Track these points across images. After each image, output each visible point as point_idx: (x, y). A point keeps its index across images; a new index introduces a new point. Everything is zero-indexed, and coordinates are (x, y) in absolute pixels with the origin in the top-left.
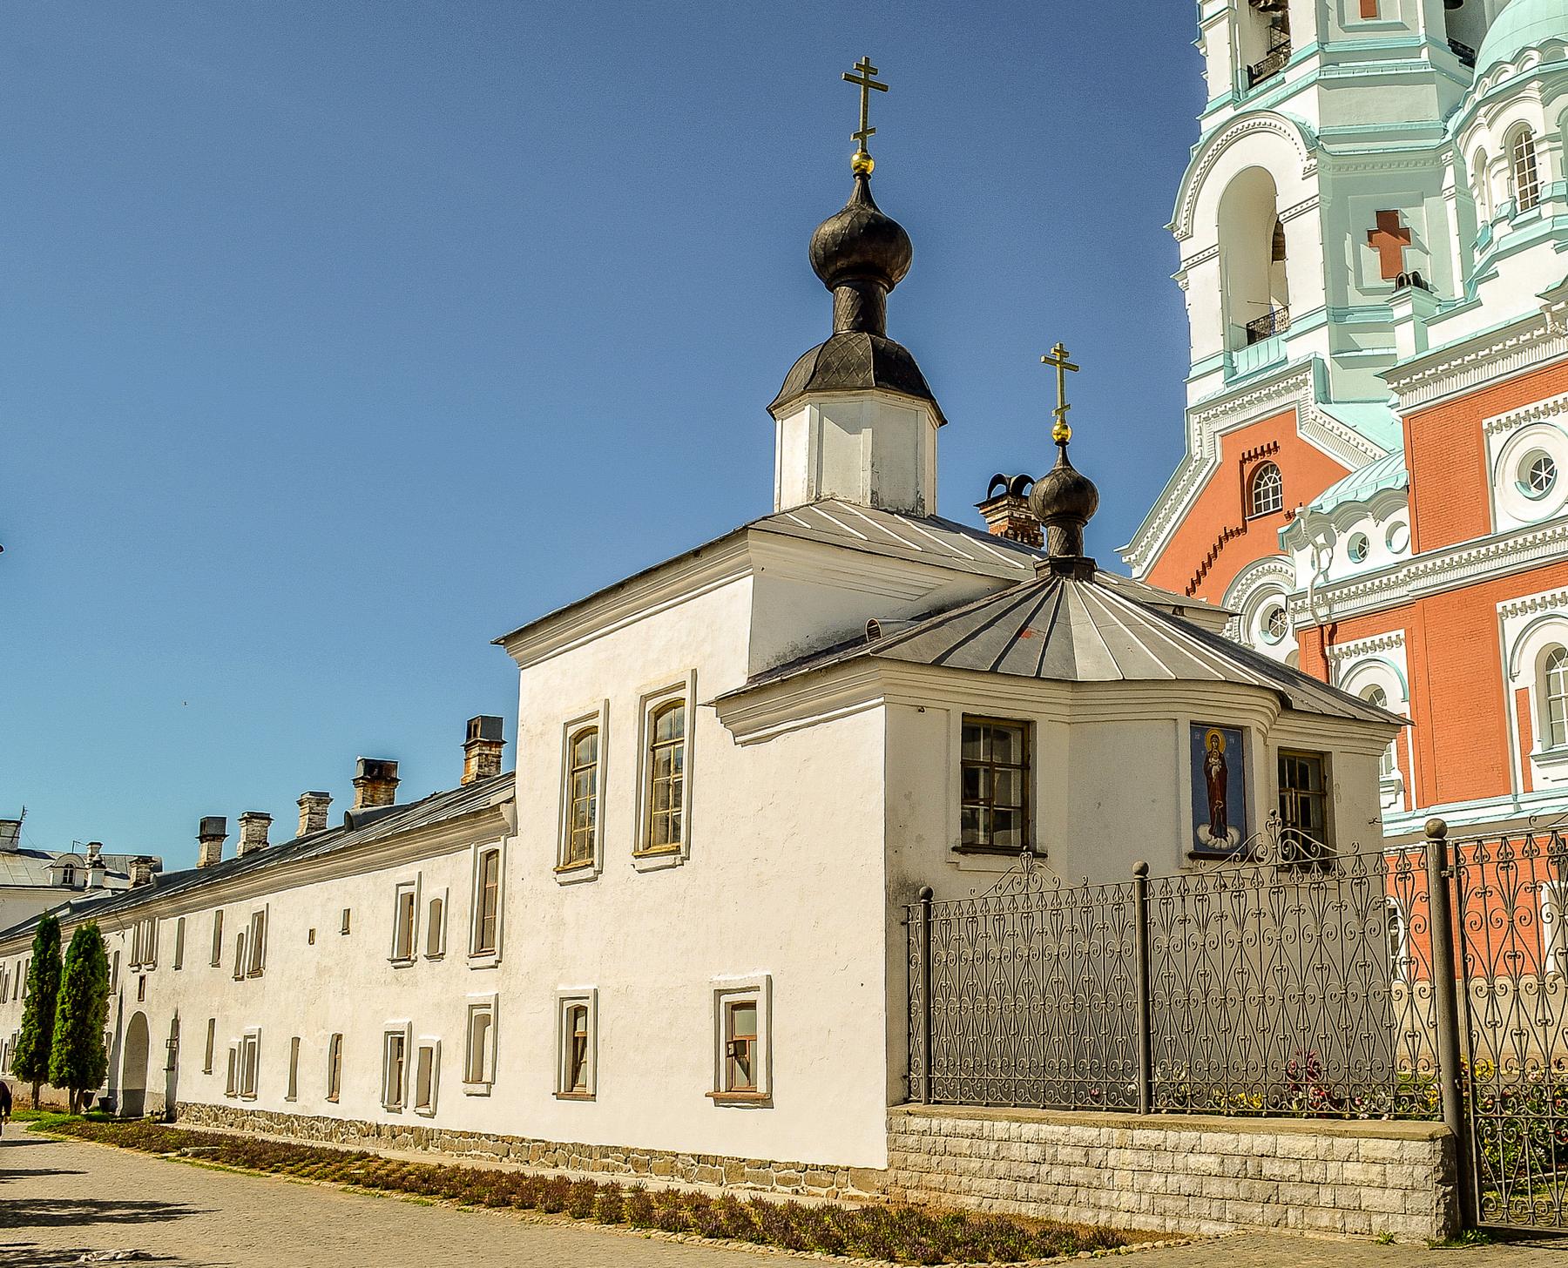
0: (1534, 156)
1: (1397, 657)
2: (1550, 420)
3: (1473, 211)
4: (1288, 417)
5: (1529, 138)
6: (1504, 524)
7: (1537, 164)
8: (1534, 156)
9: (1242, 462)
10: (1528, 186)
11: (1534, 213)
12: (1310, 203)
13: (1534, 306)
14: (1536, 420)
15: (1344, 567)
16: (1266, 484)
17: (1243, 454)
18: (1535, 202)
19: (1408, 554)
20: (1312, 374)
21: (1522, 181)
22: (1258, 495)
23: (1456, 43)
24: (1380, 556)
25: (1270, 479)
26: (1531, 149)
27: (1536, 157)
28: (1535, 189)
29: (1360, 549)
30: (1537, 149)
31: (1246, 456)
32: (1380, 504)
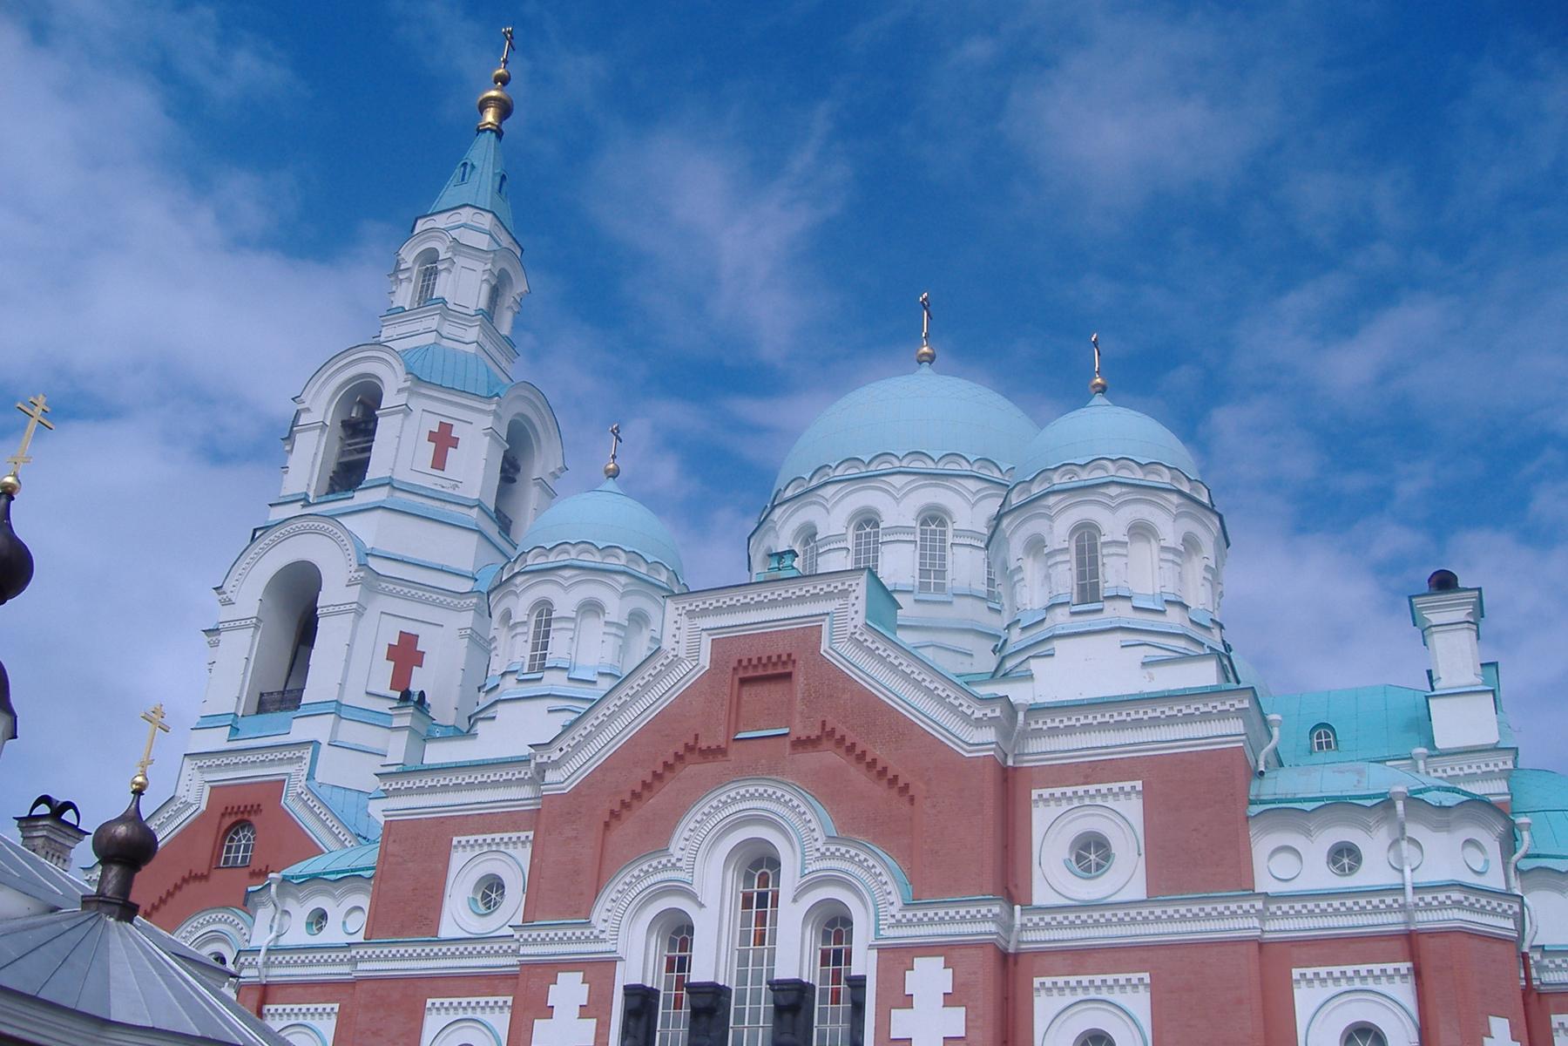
0: (546, 654)
1: (524, 855)
2: (511, 850)
3: (609, 1003)
4: (278, 786)
5: (550, 613)
6: (446, 931)
7: (551, 637)
8: (546, 654)
9: (223, 815)
10: (539, 652)
11: (539, 676)
12: (348, 607)
13: (526, 751)
14: (502, 848)
15: (297, 934)
16: (240, 840)
17: (227, 808)
18: (543, 668)
19: (359, 938)
20: (310, 754)
21: (535, 648)
22: (229, 848)
23: (500, 511)
24: (332, 934)
25: (244, 836)
26: (548, 623)
27: (548, 655)
28: (544, 657)
29: (320, 918)
30: (554, 626)
31: (229, 810)
32: (349, 878)
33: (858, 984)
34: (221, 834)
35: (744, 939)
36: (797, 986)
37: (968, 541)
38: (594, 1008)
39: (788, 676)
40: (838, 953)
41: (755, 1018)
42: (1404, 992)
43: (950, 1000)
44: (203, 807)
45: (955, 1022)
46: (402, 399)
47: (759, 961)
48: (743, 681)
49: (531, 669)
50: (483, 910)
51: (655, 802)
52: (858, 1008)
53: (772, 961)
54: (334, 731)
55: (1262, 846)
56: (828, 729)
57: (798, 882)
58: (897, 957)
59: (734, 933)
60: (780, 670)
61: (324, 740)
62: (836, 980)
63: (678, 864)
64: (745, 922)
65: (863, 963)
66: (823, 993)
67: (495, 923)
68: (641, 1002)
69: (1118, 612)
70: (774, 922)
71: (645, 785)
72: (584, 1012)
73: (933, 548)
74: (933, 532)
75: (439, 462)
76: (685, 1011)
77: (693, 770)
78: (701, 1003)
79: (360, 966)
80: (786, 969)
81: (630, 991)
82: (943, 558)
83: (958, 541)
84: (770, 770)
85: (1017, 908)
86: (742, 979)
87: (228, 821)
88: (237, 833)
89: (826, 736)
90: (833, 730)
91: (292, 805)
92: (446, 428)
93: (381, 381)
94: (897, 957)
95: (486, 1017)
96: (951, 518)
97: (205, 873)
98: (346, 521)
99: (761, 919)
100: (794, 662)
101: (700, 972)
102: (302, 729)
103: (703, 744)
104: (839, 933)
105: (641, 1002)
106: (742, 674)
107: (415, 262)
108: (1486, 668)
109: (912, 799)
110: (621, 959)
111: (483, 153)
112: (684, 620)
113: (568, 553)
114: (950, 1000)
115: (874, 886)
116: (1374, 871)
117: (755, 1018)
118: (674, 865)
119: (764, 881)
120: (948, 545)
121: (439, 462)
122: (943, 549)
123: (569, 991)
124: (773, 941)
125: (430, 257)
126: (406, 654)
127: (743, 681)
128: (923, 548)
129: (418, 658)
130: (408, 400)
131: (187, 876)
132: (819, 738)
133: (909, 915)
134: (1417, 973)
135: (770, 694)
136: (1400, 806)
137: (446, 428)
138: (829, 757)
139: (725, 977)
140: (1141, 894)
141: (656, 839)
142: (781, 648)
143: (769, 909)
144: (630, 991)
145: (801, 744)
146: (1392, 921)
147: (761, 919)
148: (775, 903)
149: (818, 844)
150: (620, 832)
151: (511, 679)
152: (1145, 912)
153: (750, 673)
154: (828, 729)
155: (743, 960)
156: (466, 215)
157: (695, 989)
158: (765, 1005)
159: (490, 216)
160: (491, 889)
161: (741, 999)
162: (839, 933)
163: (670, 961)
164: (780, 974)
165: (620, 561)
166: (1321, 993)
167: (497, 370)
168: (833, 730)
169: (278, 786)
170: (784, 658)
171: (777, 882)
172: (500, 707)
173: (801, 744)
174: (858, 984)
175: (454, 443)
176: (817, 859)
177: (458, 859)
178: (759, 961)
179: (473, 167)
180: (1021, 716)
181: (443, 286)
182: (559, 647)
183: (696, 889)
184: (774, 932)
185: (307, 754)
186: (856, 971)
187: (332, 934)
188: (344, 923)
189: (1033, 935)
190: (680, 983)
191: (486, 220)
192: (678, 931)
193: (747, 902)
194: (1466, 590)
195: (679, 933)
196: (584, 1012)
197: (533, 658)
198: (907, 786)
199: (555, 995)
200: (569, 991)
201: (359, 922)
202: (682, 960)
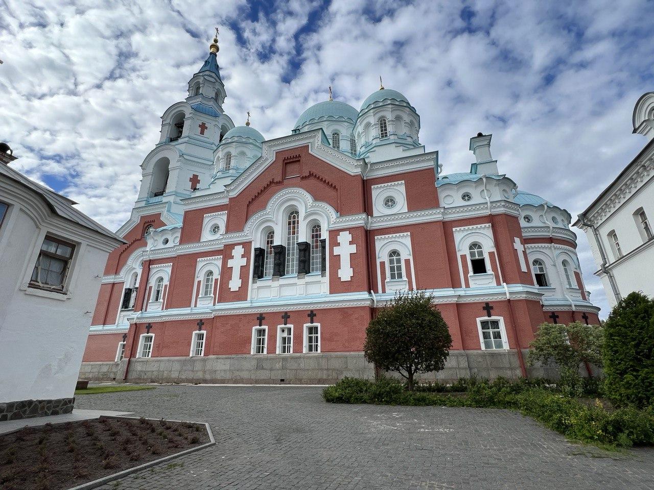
26: (230, 158)
29: (166, 241)
33: (324, 241)
35: (289, 234)
39: (299, 161)
40: (317, 235)
42: (489, 233)
43: (351, 243)
45: (353, 249)
47: (293, 239)
48: (286, 164)
49: (226, 170)
51: (262, 198)
52: (324, 248)
53: (297, 237)
55: (442, 195)
58: (334, 233)
62: (317, 242)
64: (289, 229)
65: (325, 235)
67: (217, 236)
68: (260, 253)
70: (298, 228)
72: (243, 256)
75: (202, 133)
77: (273, 187)
81: (256, 250)
84: (294, 186)
85: (369, 217)
86: (289, 244)
87: (146, 225)
88: (149, 228)
94: (334, 233)
95: (215, 262)
98: (177, 146)
99: (294, 228)
101: (277, 242)
103: (275, 181)
104: (317, 230)
105: (260, 253)
108: (477, 172)
114: (351, 243)
116: (476, 199)
119: (294, 217)
121: (202, 133)
123: (238, 251)
124: (298, 233)
129: (198, 182)
133: (338, 220)
134: (493, 226)
135: (295, 167)
136: (484, 179)
138: (312, 181)
140: (407, 211)
144: (256, 250)
145: (303, 178)
146: (487, 212)
148: (298, 223)
150: (251, 207)
152: (408, 215)
155: (289, 239)
157: (275, 247)
158: (296, 251)
160: (215, 229)
161: (289, 250)
162: (317, 230)
163: (268, 241)
166: (462, 235)
171: (298, 218)
174: (324, 241)
177: (206, 221)
180: (369, 165)
182: (233, 163)
186: (322, 238)
187: (170, 244)
189: (376, 225)
192: (270, 233)
193: (289, 224)
194: (485, 136)
195: (271, 234)
196: (243, 256)
198: (335, 187)
199: (234, 253)
200: (238, 251)
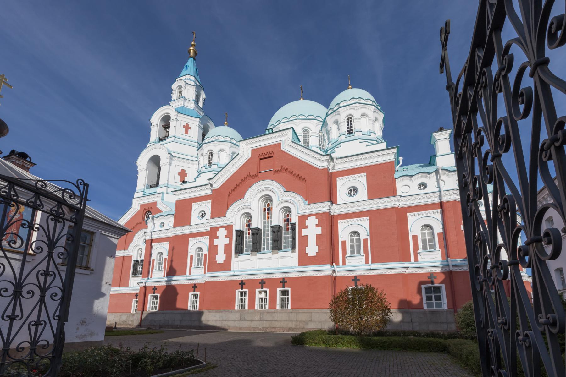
4: (155, 203)
9: (144, 210)
29: (163, 224)
33: (293, 225)
34: (144, 214)
35: (264, 218)
36: (278, 226)
37: (315, 135)
38: (229, 235)
40: (288, 220)
41: (268, 244)
43: (317, 226)
44: (139, 209)
45: (319, 231)
46: (175, 117)
47: (268, 222)
48: (261, 159)
50: (201, 218)
52: (293, 229)
54: (167, 190)
56: (283, 167)
57: (277, 203)
59: (262, 221)
60: (270, 155)
61: (165, 192)
62: (288, 224)
63: (247, 202)
64: (264, 214)
66: (285, 228)
67: (204, 220)
68: (240, 233)
69: (357, 135)
70: (272, 214)
71: (237, 185)
73: (306, 137)
74: (306, 134)
75: (187, 132)
76: (251, 235)
78: (254, 232)
79: (173, 233)
80: (275, 223)
81: (237, 231)
82: (308, 139)
83: (312, 135)
86: (264, 227)
87: (145, 211)
89: (283, 169)
90: (284, 168)
91: (159, 206)
92: (187, 125)
93: (170, 114)
96: (310, 129)
97: (141, 222)
99: (268, 213)
100: (273, 153)
101: (254, 226)
102: (158, 190)
103: (251, 174)
106: (260, 157)
107: (176, 89)
109: (306, 181)
110: (234, 224)
111: (190, 62)
112: (245, 146)
113: (215, 138)
114: (317, 226)
115: (295, 201)
117: (268, 244)
118: (246, 202)
120: (310, 136)
121: (187, 132)
122: (308, 137)
123: (222, 233)
124: (271, 218)
125: (180, 87)
126: (183, 174)
127: (261, 159)
128: (304, 137)
129: (186, 175)
130: (177, 117)
131: (137, 223)
132: (281, 170)
133: (306, 207)
137: (187, 125)
138: (284, 175)
139: (261, 226)
141: (242, 197)
142: (271, 150)
143: (270, 211)
144: (237, 231)
145: (276, 172)
147: (268, 213)
149: (282, 194)
151: (203, 168)
152: (368, 203)
153: (263, 157)
154: (283, 167)
155: (264, 223)
156: (188, 77)
159: (194, 77)
160: (203, 214)
161: (264, 231)
164: (274, 224)
165: (229, 139)
167: (198, 113)
168: (284, 168)
169: (155, 203)
170: (271, 152)
172: (201, 174)
173: (276, 172)
175: (190, 128)
176: (281, 197)
178: (268, 222)
179: (188, 66)
181: (184, 94)
182: (215, 160)
183: (251, 207)
184: (272, 216)
185: (161, 195)
186: (293, 222)
187: (166, 227)
188: (169, 225)
189: (336, 210)
190: (249, 229)
191: (193, 78)
193: (265, 210)
196: (226, 237)
197: (209, 163)
198: (304, 178)
199: (219, 234)
201: (172, 224)
202: (250, 220)
